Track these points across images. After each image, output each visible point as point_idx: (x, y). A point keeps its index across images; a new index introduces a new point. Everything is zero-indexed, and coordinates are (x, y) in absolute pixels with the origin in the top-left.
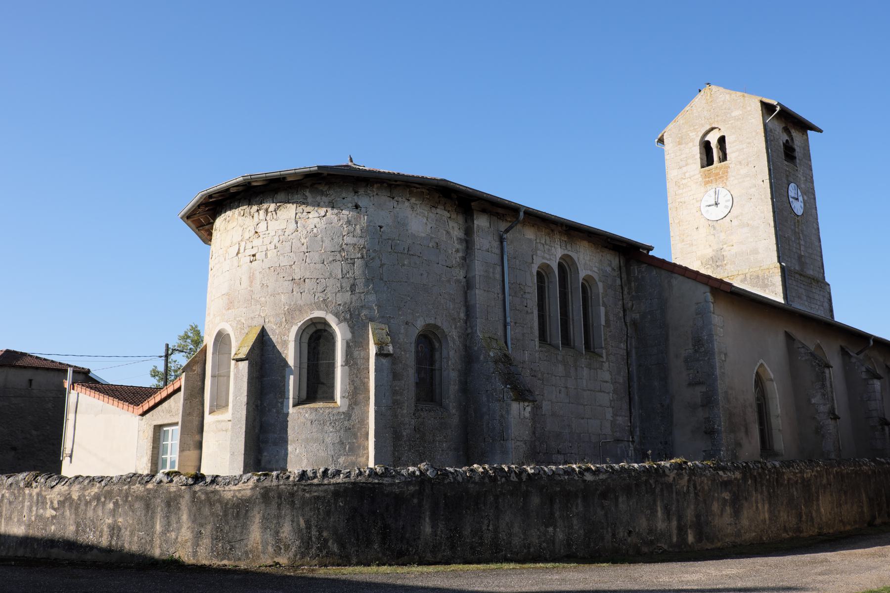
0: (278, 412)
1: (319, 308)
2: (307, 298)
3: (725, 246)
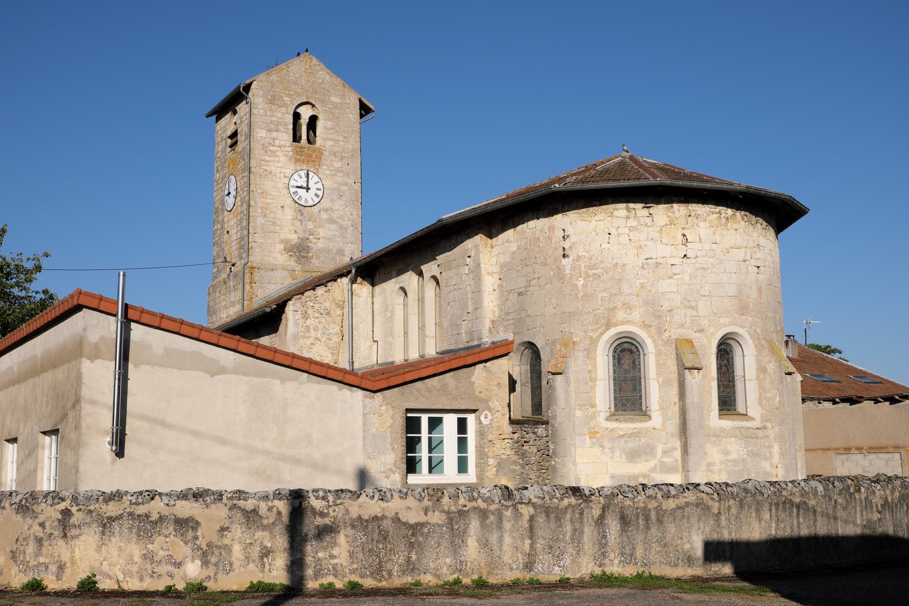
3: (311, 237)
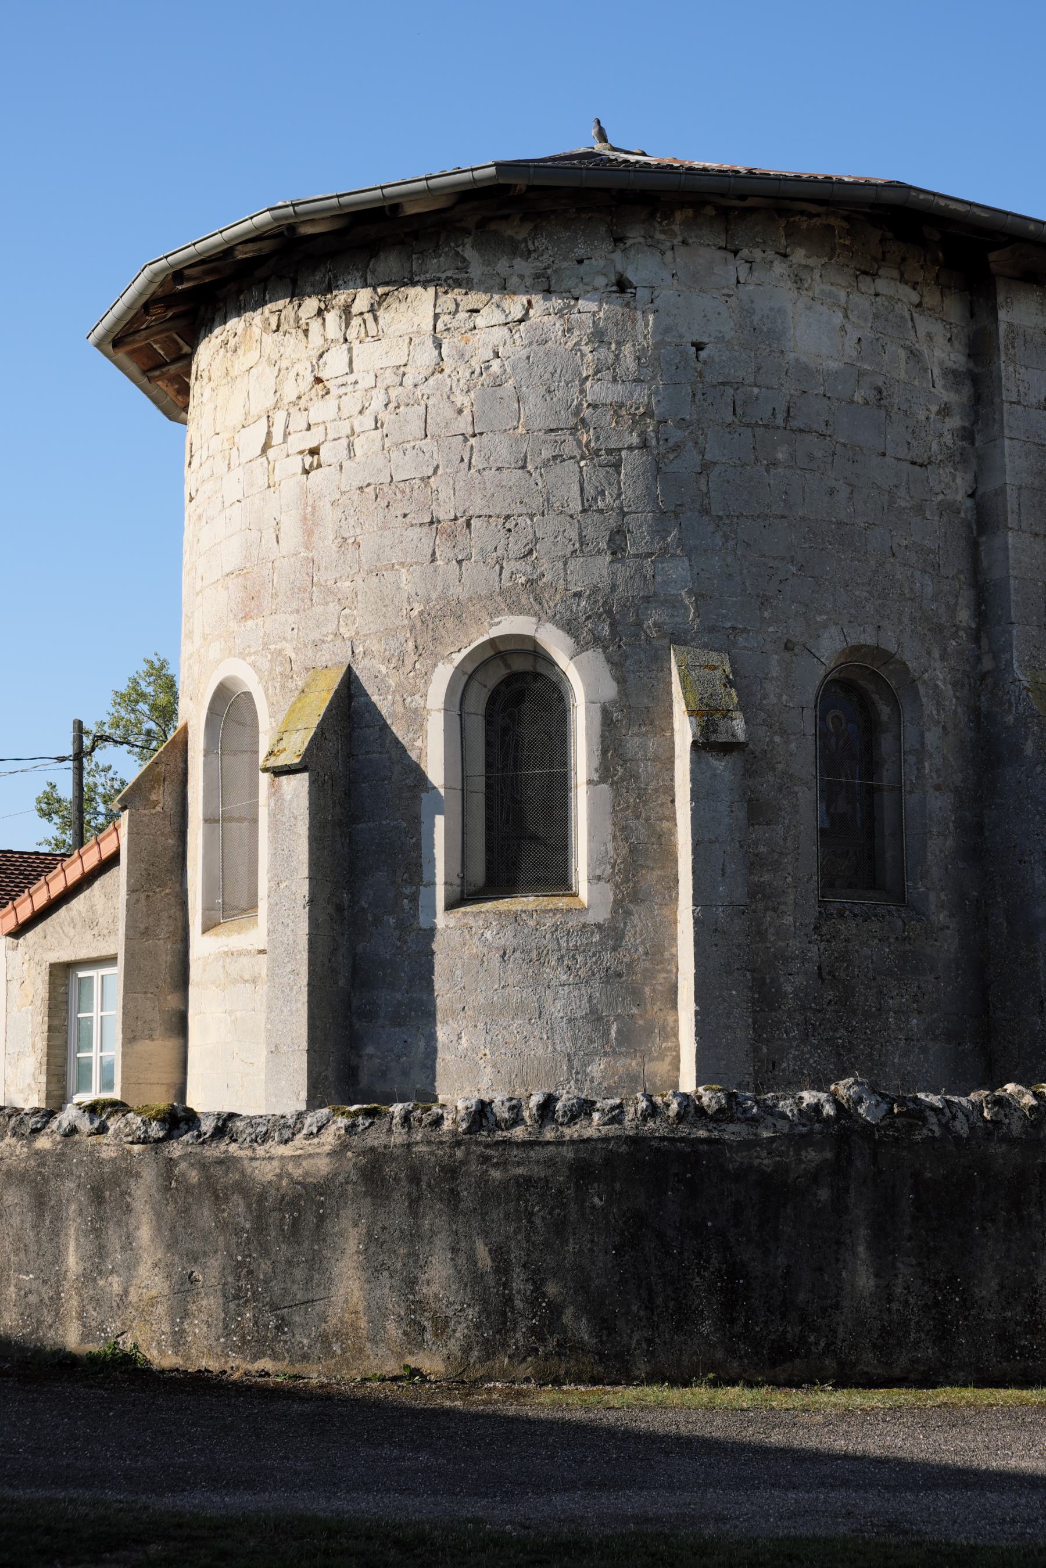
1: (515, 608)
2: (479, 576)
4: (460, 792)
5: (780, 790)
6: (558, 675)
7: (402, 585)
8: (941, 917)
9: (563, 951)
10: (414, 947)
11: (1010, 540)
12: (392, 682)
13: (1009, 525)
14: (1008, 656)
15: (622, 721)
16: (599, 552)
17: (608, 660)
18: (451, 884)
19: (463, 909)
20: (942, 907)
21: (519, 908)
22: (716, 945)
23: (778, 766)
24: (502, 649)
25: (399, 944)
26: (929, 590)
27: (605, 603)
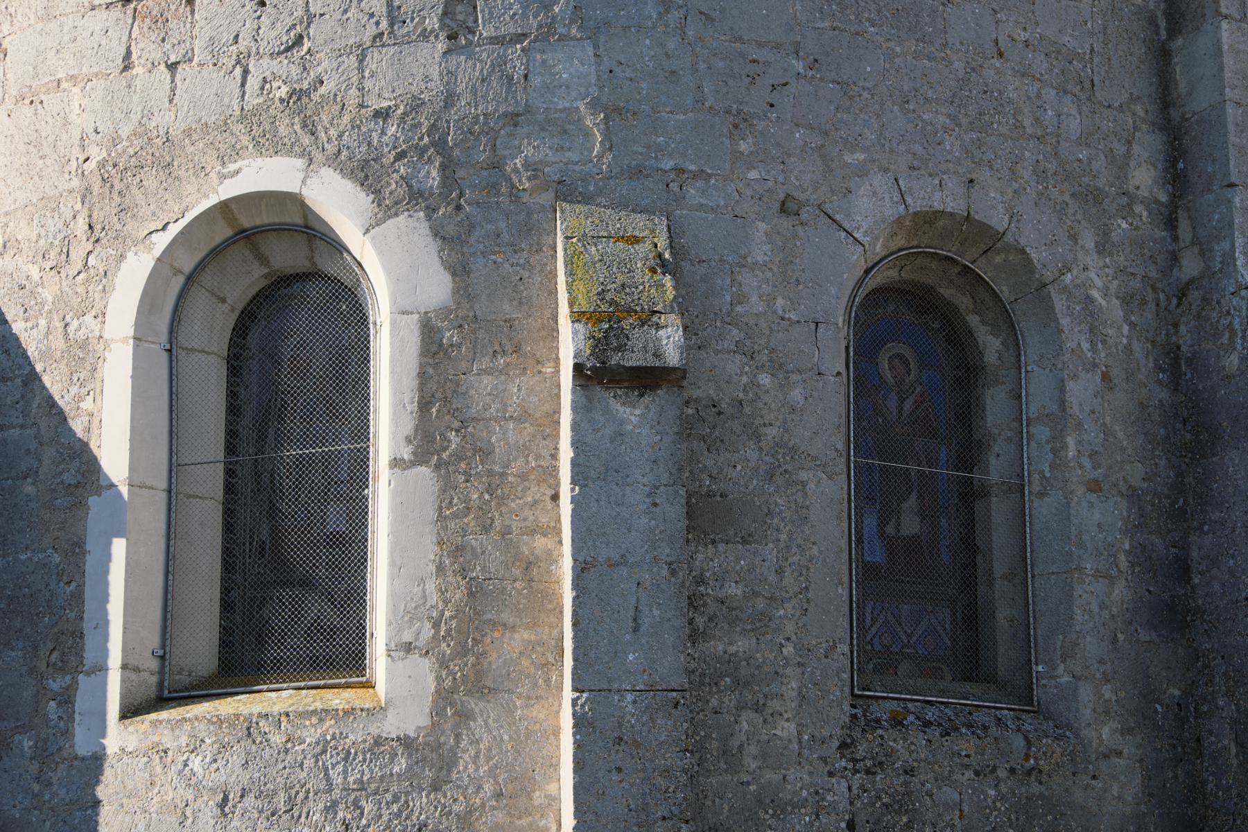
0: (46, 754)
1: (267, 143)
2: (207, 90)
4: (164, 495)
5: (770, 476)
6: (346, 267)
7: (73, 117)
8: (1105, 732)
9: (336, 794)
10: (62, 792)
11: (1225, 35)
12: (47, 295)
13: (1224, 10)
14: (1225, 245)
15: (459, 346)
16: (425, 35)
17: (436, 233)
18: (137, 670)
19: (153, 716)
20: (1106, 713)
21: (256, 709)
22: (619, 770)
23: (768, 430)
24: (247, 225)
25: (36, 787)
26: (1074, 125)
27: (433, 128)
